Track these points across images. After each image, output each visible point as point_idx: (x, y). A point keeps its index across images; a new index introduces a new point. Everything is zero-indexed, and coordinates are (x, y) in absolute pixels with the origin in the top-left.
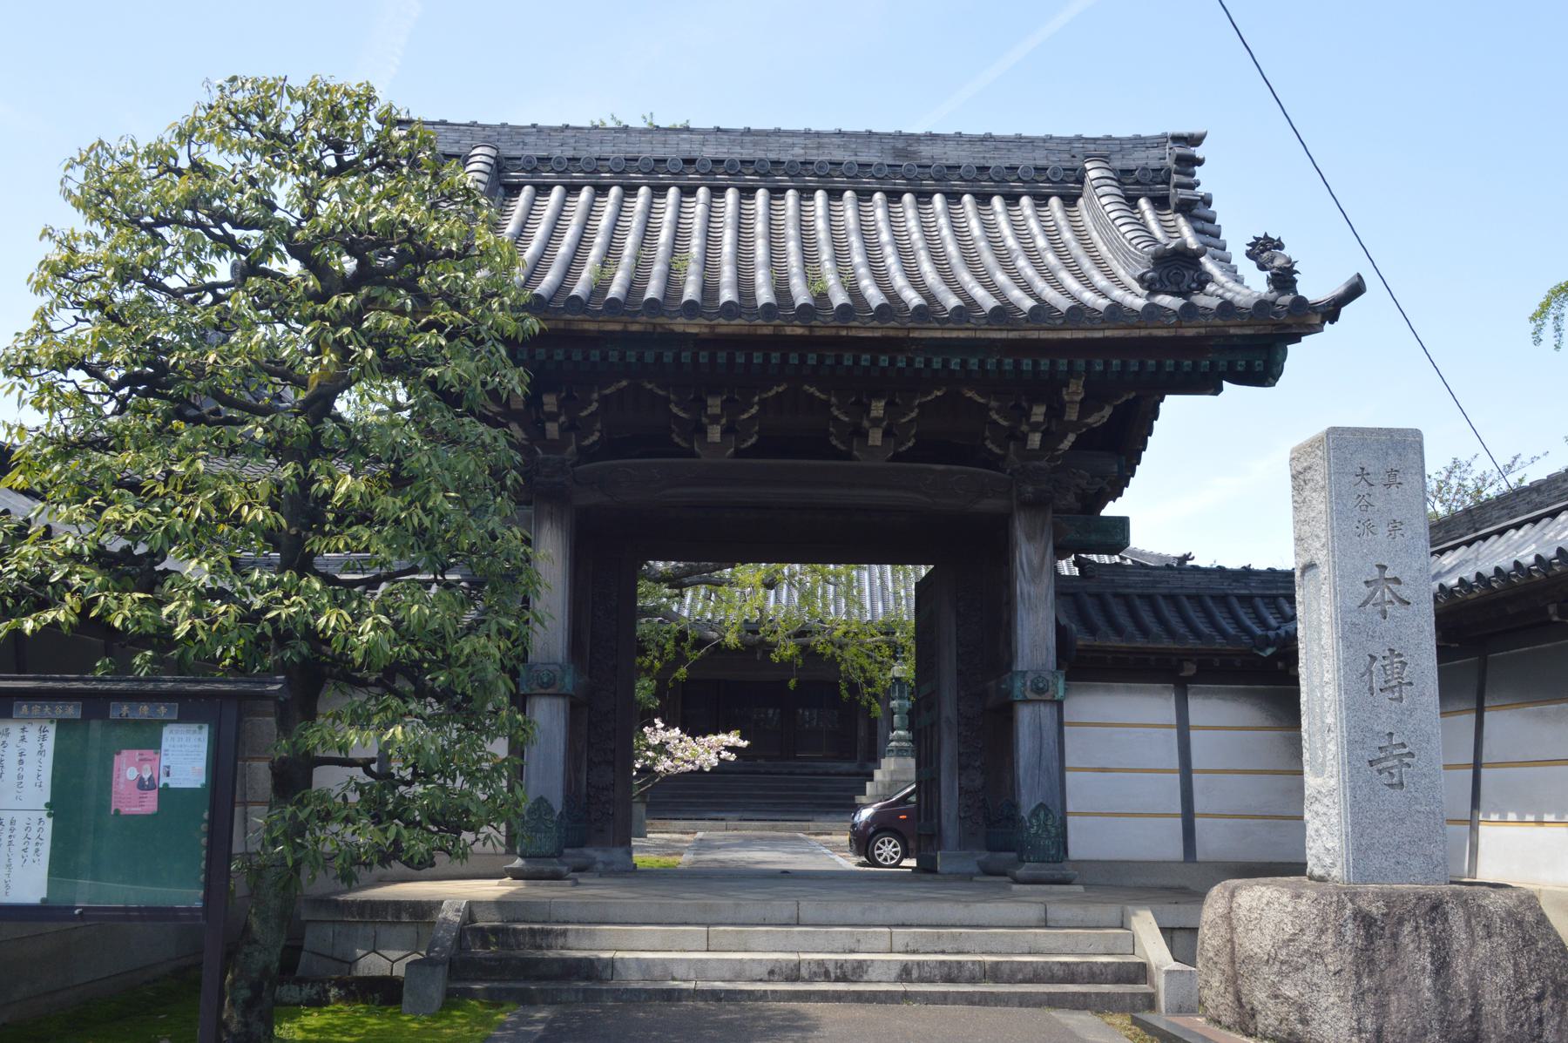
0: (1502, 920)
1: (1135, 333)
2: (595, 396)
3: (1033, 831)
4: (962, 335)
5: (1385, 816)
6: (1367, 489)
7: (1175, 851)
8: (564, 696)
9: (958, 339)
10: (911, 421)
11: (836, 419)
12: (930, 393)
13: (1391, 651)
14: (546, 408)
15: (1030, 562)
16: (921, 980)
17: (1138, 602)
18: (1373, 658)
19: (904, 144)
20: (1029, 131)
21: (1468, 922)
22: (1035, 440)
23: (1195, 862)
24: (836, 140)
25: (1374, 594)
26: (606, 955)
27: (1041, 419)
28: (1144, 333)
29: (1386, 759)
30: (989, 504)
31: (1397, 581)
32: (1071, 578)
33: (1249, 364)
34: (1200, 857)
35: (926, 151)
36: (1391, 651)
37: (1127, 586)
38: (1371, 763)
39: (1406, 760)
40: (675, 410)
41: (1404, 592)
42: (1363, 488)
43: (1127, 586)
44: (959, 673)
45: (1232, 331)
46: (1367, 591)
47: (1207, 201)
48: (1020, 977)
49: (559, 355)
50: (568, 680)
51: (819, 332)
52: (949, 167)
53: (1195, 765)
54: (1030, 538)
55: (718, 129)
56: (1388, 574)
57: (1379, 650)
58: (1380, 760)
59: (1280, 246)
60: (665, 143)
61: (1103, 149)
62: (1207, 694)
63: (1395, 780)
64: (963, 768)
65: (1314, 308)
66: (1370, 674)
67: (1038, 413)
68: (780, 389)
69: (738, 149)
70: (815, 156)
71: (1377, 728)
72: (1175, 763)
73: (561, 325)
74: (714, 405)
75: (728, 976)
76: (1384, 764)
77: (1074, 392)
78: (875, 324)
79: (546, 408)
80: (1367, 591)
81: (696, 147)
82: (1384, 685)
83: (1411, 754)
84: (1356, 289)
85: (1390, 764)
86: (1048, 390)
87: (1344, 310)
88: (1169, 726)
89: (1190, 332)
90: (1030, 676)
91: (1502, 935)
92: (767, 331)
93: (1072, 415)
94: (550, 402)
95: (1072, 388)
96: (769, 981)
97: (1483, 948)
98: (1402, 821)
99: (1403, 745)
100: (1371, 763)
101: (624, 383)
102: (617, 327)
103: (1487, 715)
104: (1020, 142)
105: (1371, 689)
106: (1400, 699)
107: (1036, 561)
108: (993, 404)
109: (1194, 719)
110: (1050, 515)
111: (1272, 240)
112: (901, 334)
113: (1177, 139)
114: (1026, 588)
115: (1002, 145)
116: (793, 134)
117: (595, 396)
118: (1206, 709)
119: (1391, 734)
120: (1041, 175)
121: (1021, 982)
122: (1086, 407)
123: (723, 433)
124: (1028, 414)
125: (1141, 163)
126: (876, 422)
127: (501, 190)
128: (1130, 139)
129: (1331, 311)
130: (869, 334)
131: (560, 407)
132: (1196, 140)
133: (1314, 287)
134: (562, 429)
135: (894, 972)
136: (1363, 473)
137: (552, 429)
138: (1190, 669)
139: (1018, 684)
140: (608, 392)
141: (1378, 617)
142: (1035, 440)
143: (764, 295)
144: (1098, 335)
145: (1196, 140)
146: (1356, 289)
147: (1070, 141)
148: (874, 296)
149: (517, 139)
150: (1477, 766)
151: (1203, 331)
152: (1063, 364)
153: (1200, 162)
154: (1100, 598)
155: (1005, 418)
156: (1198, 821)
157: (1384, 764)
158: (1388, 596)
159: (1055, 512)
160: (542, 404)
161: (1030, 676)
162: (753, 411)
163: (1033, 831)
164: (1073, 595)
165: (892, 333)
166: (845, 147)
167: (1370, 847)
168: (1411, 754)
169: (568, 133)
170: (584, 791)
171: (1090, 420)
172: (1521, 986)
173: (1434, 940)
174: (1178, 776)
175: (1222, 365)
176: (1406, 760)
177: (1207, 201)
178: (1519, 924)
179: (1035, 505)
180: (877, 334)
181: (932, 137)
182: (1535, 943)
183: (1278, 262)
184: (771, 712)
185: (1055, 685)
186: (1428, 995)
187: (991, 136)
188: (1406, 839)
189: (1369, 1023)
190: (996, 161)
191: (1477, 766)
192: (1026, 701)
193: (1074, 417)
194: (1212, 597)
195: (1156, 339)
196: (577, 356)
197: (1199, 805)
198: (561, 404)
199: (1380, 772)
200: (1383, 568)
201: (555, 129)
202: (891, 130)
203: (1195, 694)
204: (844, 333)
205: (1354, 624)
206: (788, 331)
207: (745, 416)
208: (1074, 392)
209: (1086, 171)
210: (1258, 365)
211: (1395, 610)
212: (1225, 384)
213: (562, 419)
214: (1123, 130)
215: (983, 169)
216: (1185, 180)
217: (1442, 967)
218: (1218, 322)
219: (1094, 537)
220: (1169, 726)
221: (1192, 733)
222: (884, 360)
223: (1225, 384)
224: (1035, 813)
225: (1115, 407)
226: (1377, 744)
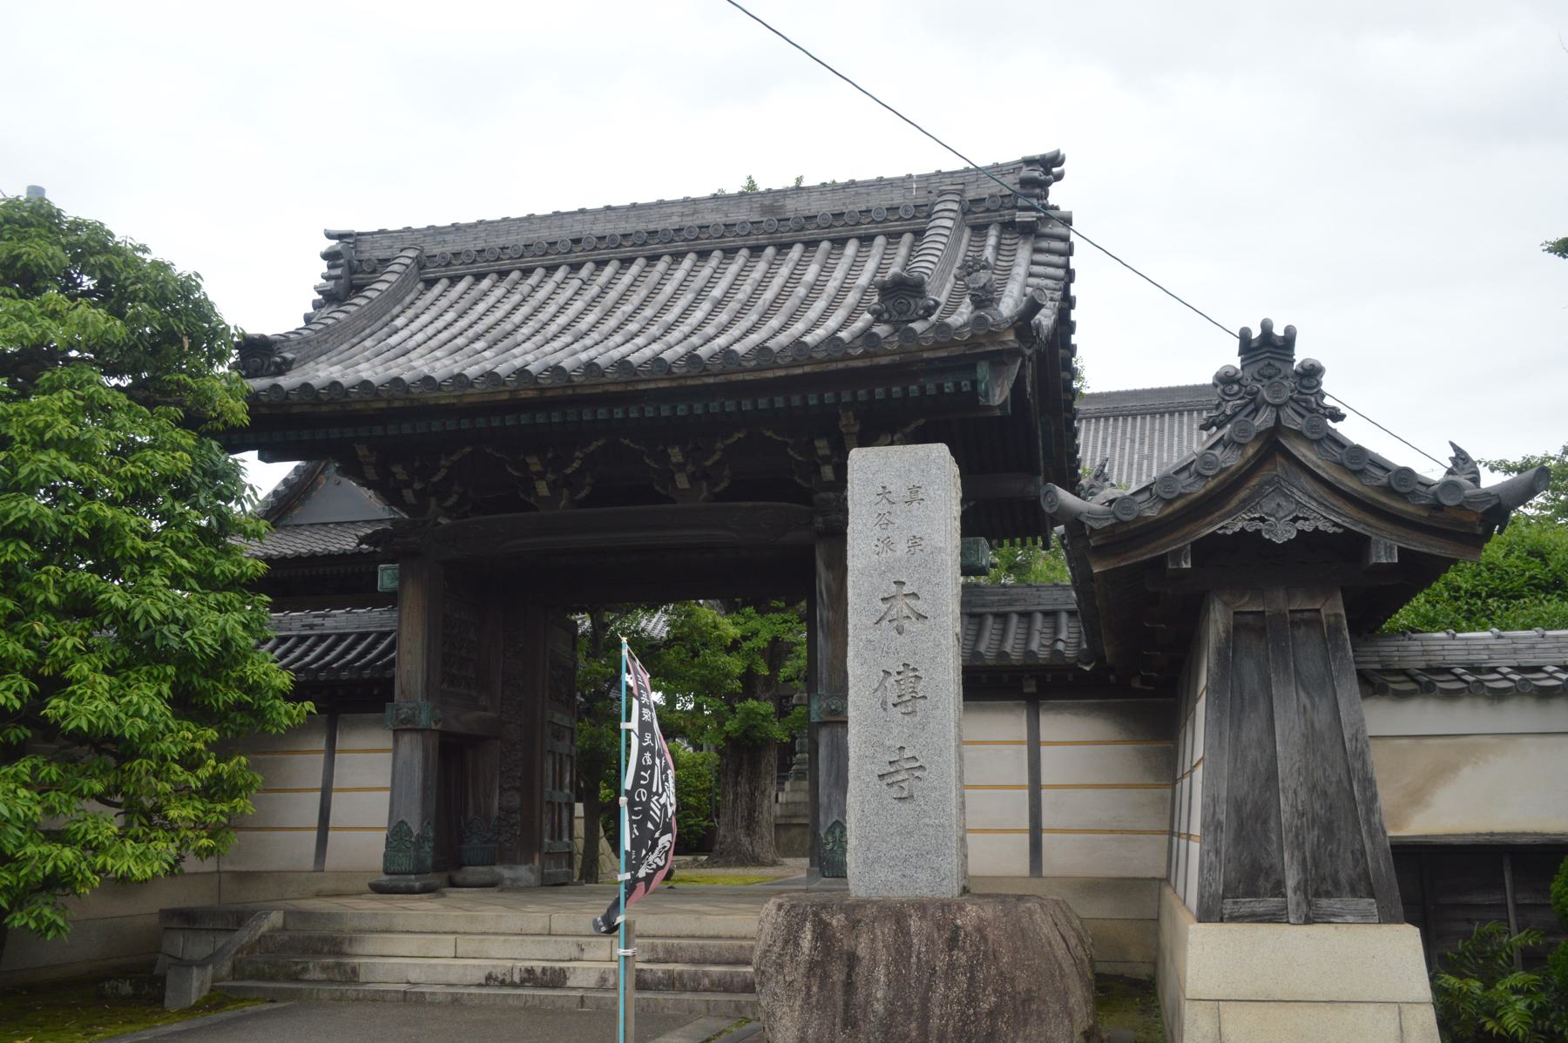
3: (829, 847)
5: (892, 829)
6: (888, 507)
7: (1021, 866)
9: (744, 381)
14: (674, 460)
15: (828, 588)
19: (772, 201)
23: (1041, 876)
24: (710, 205)
34: (1045, 872)
35: (791, 206)
37: (983, 606)
38: (881, 777)
41: (920, 606)
42: (884, 507)
46: (884, 607)
52: (806, 218)
53: (1045, 780)
60: (561, 227)
62: (1058, 709)
68: (600, 443)
69: (623, 224)
70: (688, 222)
71: (888, 743)
72: (1025, 779)
79: (674, 460)
81: (587, 227)
82: (897, 700)
85: (900, 778)
94: (399, 471)
98: (910, 833)
101: (468, 449)
105: (884, 703)
108: (790, 441)
109: (1044, 735)
115: (863, 190)
116: (673, 203)
117: (719, 445)
118: (1057, 726)
119: (902, 748)
138: (1030, 688)
141: (894, 633)
149: (439, 238)
151: (897, 358)
156: (1045, 836)
158: (906, 612)
160: (815, 448)
162: (576, 465)
163: (829, 847)
166: (717, 210)
167: (877, 860)
169: (481, 227)
174: (1026, 792)
188: (913, 853)
195: (708, 385)
196: (879, 393)
197: (1047, 820)
200: (900, 583)
201: (470, 226)
203: (1048, 710)
205: (869, 641)
211: (912, 626)
220: (1020, 743)
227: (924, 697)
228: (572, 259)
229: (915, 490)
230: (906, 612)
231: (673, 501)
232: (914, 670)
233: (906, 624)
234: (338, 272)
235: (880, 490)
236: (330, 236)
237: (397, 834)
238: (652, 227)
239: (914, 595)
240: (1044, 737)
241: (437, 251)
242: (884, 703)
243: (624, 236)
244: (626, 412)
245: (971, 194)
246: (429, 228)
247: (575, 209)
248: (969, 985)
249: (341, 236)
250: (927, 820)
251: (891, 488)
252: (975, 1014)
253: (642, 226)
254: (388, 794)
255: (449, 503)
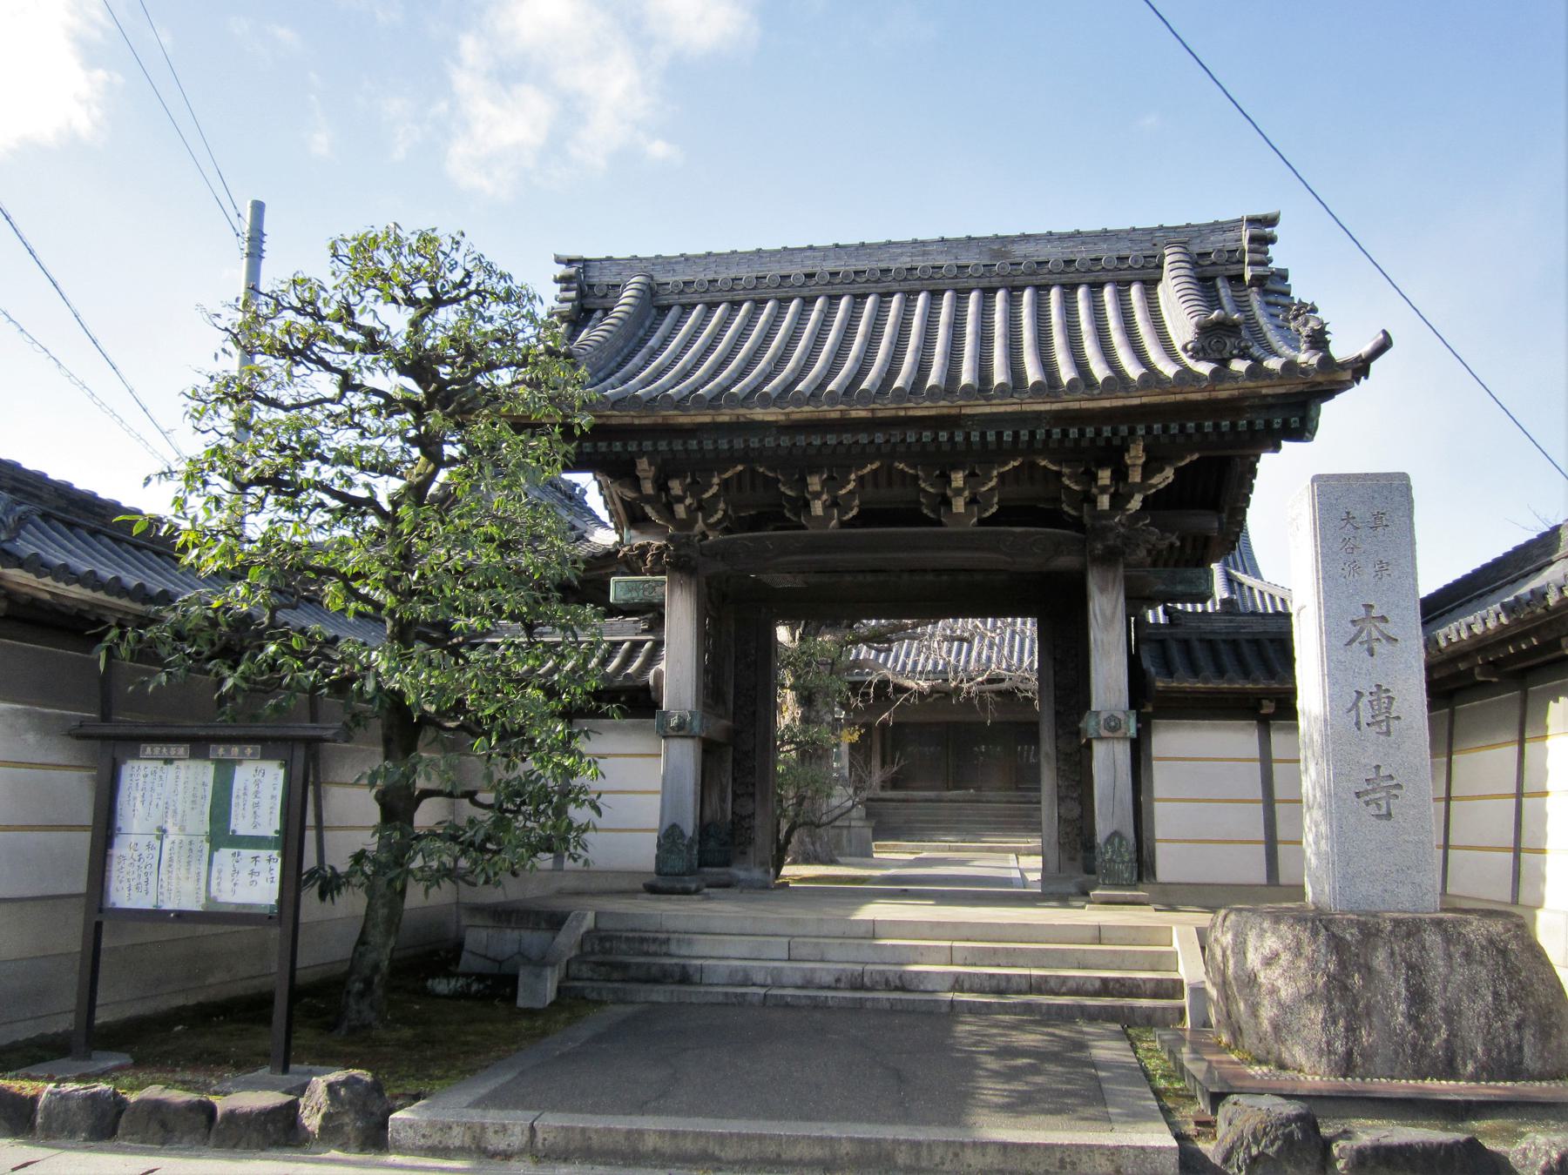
0: (1483, 948)
1: (1171, 398)
2: (853, 476)
4: (1009, 409)
8: (693, 737)
9: (1006, 413)
10: (991, 489)
11: (924, 490)
12: (1006, 464)
13: (1379, 686)
16: (971, 990)
17: (1222, 647)
18: (1359, 694)
20: (1113, 225)
21: (1446, 950)
22: (1104, 502)
25: (1361, 631)
26: (698, 962)
27: (1107, 482)
28: (1179, 397)
29: (1374, 790)
30: (1066, 562)
31: (1383, 619)
32: (1157, 624)
33: (1286, 422)
35: (1019, 250)
36: (1379, 686)
38: (1358, 795)
39: (1394, 792)
40: (783, 489)
41: (1390, 629)
43: (1213, 632)
44: (1057, 713)
45: (1264, 391)
47: (1282, 276)
48: (1064, 989)
49: (1107, 431)
50: (696, 724)
51: (880, 414)
52: (1039, 263)
53: (1278, 795)
54: (1102, 590)
55: (837, 246)
56: (1374, 613)
57: (1366, 686)
58: (1367, 792)
59: (1314, 310)
61: (1182, 236)
63: (1384, 811)
64: (1061, 799)
65: (1343, 366)
66: (1364, 709)
67: (1105, 477)
68: (1016, 464)
70: (920, 263)
73: (660, 420)
74: (958, 479)
75: (799, 983)
76: (1372, 796)
77: (1136, 456)
78: (927, 404)
80: (1354, 630)
82: (1370, 720)
83: (1398, 786)
84: (1384, 346)
86: (1114, 457)
87: (1373, 365)
88: (1253, 760)
89: (1223, 395)
90: (1103, 716)
91: (1482, 963)
92: (835, 415)
93: (1135, 476)
94: (676, 487)
95: (1133, 453)
96: (836, 989)
97: (1461, 974)
99: (1391, 777)
100: (1358, 795)
101: (740, 468)
102: (707, 419)
103: (1527, 745)
104: (1105, 235)
105: (1358, 724)
106: (1388, 733)
107: (1108, 612)
108: (1066, 470)
110: (1121, 570)
111: (1305, 305)
112: (954, 411)
113: (1252, 221)
114: (1099, 637)
117: (853, 476)
119: (1378, 767)
120: (1125, 265)
121: (1064, 994)
122: (1149, 470)
123: (967, 504)
124: (1095, 478)
125: (1219, 246)
126: (1103, 490)
127: (654, 311)
128: (1208, 225)
129: (1360, 368)
130: (925, 413)
131: (685, 492)
132: (1272, 221)
133: (1343, 348)
134: (826, 507)
135: (948, 983)
136: (1349, 517)
137: (680, 511)
139: (1093, 723)
140: (726, 476)
142: (1104, 502)
143: (1066, 373)
144: (1136, 401)
145: (1272, 221)
146: (1384, 346)
147: (1151, 231)
148: (1133, 371)
150: (1448, 798)
152: (1124, 430)
153: (1272, 240)
154: (1186, 644)
155: (1077, 483)
157: (1372, 796)
159: (1127, 566)
161: (1103, 716)
162: (851, 486)
163: (1108, 856)
164: (1210, 641)
165: (945, 411)
168: (1398, 786)
170: (729, 817)
171: (1154, 481)
172: (1500, 1013)
173: (1410, 967)
175: (1277, 423)
176: (1394, 792)
177: (1282, 276)
178: (1503, 952)
179: (1109, 558)
180: (933, 412)
181: (1025, 238)
182: (1519, 972)
183: (1312, 324)
184: (559, 728)
185: (1127, 723)
186: (1401, 1019)
187: (1079, 232)
188: (1394, 869)
189: (1339, 1047)
190: (1082, 254)
191: (1448, 798)
192: (1100, 738)
193: (1138, 479)
194: (1201, 641)
198: (824, 483)
199: (1367, 803)
200: (1369, 607)
202: (990, 234)
204: (902, 413)
206: (854, 414)
207: (843, 492)
208: (1136, 456)
209: (1163, 256)
210: (1294, 422)
211: (1381, 648)
212: (1284, 443)
213: (825, 497)
214: (1202, 216)
215: (1069, 262)
216: (1258, 257)
217: (1418, 998)
218: (1251, 384)
219: (1180, 588)
220: (1253, 760)
221: (1275, 766)
222: (943, 436)
223: (1284, 443)
224: (1109, 840)
225: (1177, 471)
226: (1364, 776)
227: (1398, 718)
228: (806, 292)
229: (1378, 516)
230: (1375, 634)
231: (803, 527)
232: (1387, 691)
233: (1376, 645)
234: (573, 294)
235: (1344, 516)
236: (559, 261)
237: (670, 837)
238: (884, 265)
239: (1383, 619)
240: (1275, 755)
241: (670, 279)
242: (1358, 724)
243: (856, 273)
244: (625, 445)
245: (1196, 249)
246: (657, 257)
247: (805, 245)
248: (1494, 999)
249: (570, 262)
250: (1406, 837)
251: (1354, 513)
252: (1503, 1027)
253: (874, 265)
254: (659, 797)
255: (712, 520)
